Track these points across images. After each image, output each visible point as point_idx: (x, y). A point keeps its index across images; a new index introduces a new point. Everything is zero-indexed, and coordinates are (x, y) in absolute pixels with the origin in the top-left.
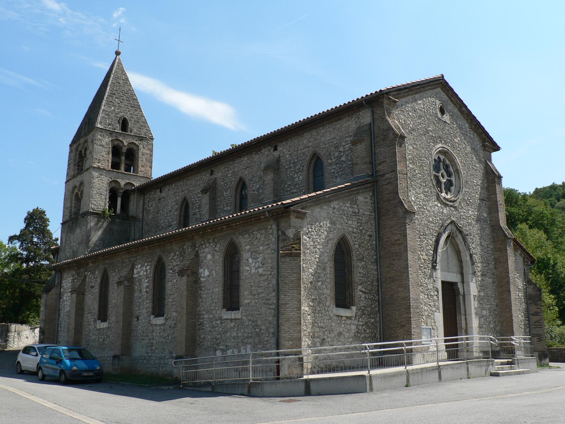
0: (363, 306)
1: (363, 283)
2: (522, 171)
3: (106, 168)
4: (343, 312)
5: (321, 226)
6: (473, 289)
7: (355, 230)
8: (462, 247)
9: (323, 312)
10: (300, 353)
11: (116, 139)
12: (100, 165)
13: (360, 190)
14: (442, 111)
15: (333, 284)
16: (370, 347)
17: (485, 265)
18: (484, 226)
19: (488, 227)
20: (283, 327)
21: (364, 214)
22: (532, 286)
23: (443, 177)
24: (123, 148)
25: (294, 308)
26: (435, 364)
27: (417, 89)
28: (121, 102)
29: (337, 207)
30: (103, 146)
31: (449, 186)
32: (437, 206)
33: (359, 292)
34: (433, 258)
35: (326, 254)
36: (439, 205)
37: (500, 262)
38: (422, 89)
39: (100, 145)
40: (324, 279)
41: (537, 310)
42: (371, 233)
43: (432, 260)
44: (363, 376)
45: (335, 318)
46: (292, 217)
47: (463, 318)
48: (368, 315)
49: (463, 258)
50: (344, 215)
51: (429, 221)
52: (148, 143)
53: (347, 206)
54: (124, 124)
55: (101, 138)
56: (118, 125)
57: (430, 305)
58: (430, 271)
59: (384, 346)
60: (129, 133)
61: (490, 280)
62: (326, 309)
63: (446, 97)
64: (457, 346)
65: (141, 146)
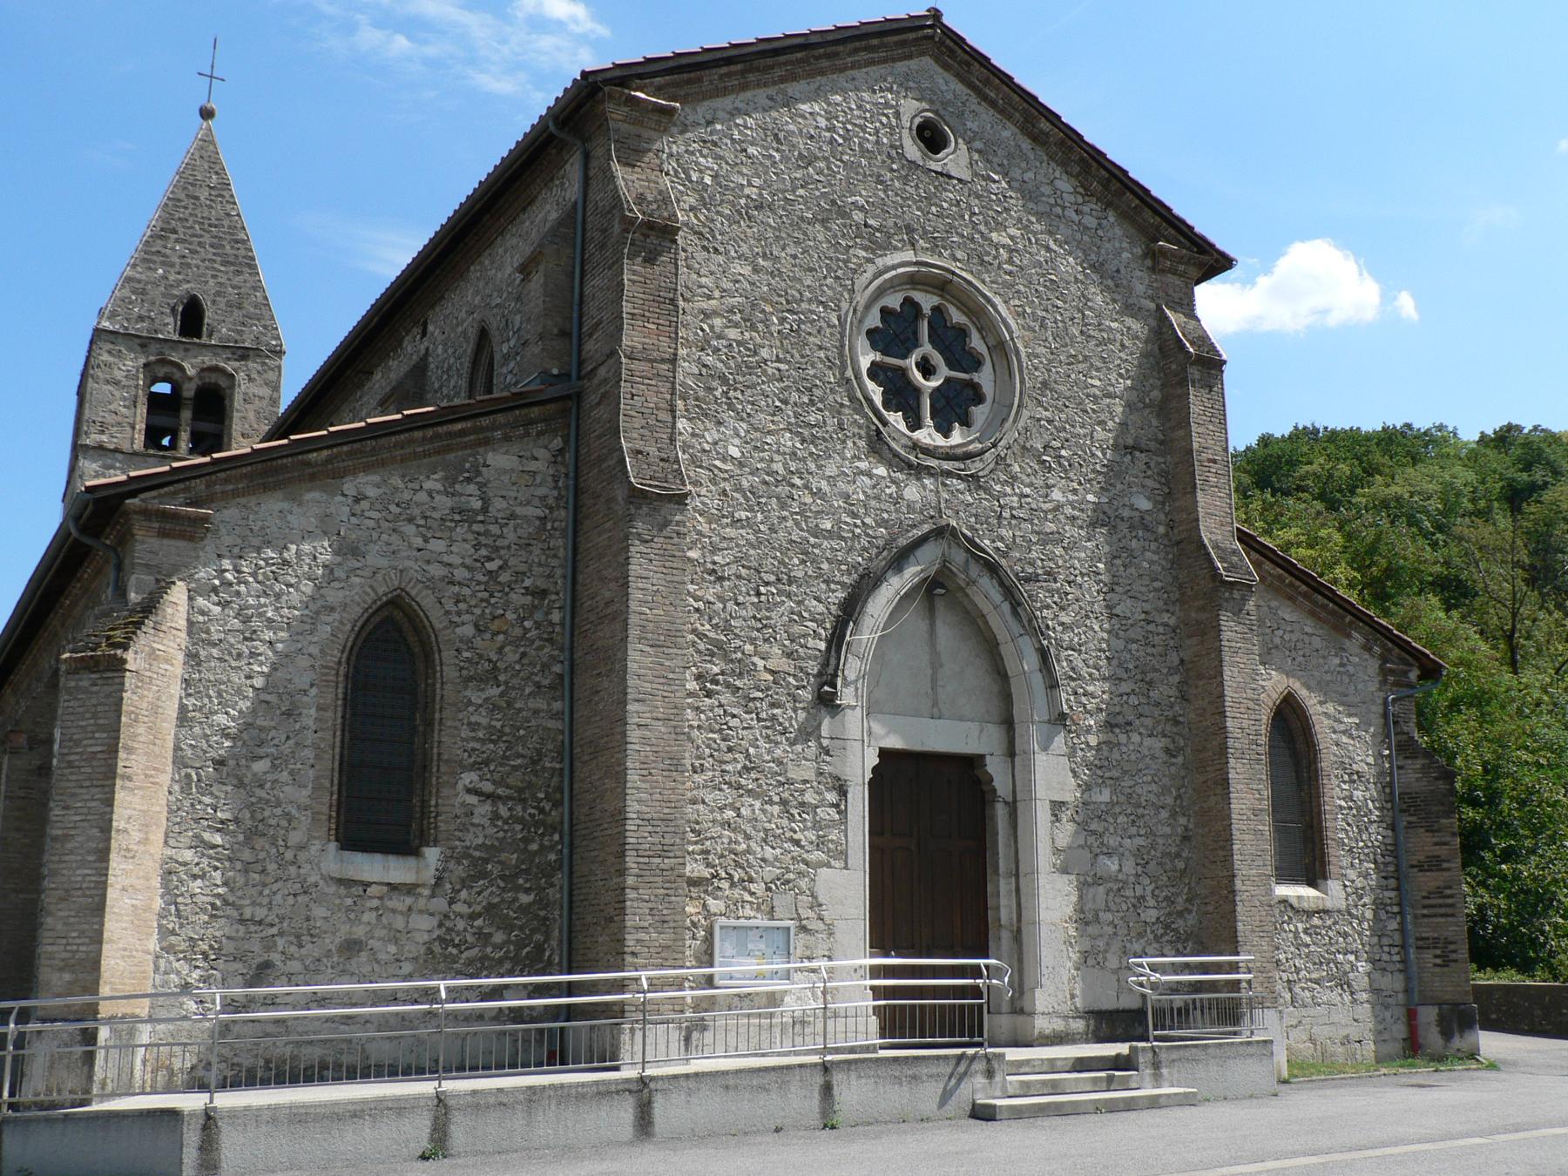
0: (477, 848)
1: (487, 763)
2: (1312, 330)
3: (126, 447)
4: (374, 868)
5: (286, 563)
6: (1052, 776)
7: (461, 574)
8: (1000, 621)
9: (272, 867)
10: (91, 1011)
11: (158, 361)
12: (104, 438)
13: (493, 428)
14: (931, 138)
15: (330, 762)
16: (518, 991)
17: (1125, 687)
18: (1134, 544)
19: (1153, 546)
20: (49, 920)
21: (513, 516)
22: (1419, 763)
23: (927, 369)
24: (186, 386)
25: (89, 853)
26: (815, 1059)
27: (792, 63)
28: (191, 251)
29: (372, 492)
30: (117, 383)
31: (954, 405)
32: (869, 475)
33: (463, 797)
34: (826, 664)
35: (303, 662)
36: (881, 471)
37: (1200, 676)
38: (825, 63)
39: (108, 382)
40: (286, 748)
41: (1437, 850)
42: (542, 584)
43: (820, 674)
44: (173, 1114)
45: (332, 889)
46: (139, 533)
47: (1005, 886)
48: (502, 877)
49: (1011, 666)
50: (411, 520)
51: (816, 532)
52: (264, 364)
53: (430, 490)
54: (192, 317)
55: (111, 359)
56: (170, 320)
57: (797, 843)
58: (802, 715)
59: (570, 988)
60: (204, 340)
61: (1148, 742)
62: (289, 855)
63: (960, 88)
64: (976, 992)
65: (241, 377)
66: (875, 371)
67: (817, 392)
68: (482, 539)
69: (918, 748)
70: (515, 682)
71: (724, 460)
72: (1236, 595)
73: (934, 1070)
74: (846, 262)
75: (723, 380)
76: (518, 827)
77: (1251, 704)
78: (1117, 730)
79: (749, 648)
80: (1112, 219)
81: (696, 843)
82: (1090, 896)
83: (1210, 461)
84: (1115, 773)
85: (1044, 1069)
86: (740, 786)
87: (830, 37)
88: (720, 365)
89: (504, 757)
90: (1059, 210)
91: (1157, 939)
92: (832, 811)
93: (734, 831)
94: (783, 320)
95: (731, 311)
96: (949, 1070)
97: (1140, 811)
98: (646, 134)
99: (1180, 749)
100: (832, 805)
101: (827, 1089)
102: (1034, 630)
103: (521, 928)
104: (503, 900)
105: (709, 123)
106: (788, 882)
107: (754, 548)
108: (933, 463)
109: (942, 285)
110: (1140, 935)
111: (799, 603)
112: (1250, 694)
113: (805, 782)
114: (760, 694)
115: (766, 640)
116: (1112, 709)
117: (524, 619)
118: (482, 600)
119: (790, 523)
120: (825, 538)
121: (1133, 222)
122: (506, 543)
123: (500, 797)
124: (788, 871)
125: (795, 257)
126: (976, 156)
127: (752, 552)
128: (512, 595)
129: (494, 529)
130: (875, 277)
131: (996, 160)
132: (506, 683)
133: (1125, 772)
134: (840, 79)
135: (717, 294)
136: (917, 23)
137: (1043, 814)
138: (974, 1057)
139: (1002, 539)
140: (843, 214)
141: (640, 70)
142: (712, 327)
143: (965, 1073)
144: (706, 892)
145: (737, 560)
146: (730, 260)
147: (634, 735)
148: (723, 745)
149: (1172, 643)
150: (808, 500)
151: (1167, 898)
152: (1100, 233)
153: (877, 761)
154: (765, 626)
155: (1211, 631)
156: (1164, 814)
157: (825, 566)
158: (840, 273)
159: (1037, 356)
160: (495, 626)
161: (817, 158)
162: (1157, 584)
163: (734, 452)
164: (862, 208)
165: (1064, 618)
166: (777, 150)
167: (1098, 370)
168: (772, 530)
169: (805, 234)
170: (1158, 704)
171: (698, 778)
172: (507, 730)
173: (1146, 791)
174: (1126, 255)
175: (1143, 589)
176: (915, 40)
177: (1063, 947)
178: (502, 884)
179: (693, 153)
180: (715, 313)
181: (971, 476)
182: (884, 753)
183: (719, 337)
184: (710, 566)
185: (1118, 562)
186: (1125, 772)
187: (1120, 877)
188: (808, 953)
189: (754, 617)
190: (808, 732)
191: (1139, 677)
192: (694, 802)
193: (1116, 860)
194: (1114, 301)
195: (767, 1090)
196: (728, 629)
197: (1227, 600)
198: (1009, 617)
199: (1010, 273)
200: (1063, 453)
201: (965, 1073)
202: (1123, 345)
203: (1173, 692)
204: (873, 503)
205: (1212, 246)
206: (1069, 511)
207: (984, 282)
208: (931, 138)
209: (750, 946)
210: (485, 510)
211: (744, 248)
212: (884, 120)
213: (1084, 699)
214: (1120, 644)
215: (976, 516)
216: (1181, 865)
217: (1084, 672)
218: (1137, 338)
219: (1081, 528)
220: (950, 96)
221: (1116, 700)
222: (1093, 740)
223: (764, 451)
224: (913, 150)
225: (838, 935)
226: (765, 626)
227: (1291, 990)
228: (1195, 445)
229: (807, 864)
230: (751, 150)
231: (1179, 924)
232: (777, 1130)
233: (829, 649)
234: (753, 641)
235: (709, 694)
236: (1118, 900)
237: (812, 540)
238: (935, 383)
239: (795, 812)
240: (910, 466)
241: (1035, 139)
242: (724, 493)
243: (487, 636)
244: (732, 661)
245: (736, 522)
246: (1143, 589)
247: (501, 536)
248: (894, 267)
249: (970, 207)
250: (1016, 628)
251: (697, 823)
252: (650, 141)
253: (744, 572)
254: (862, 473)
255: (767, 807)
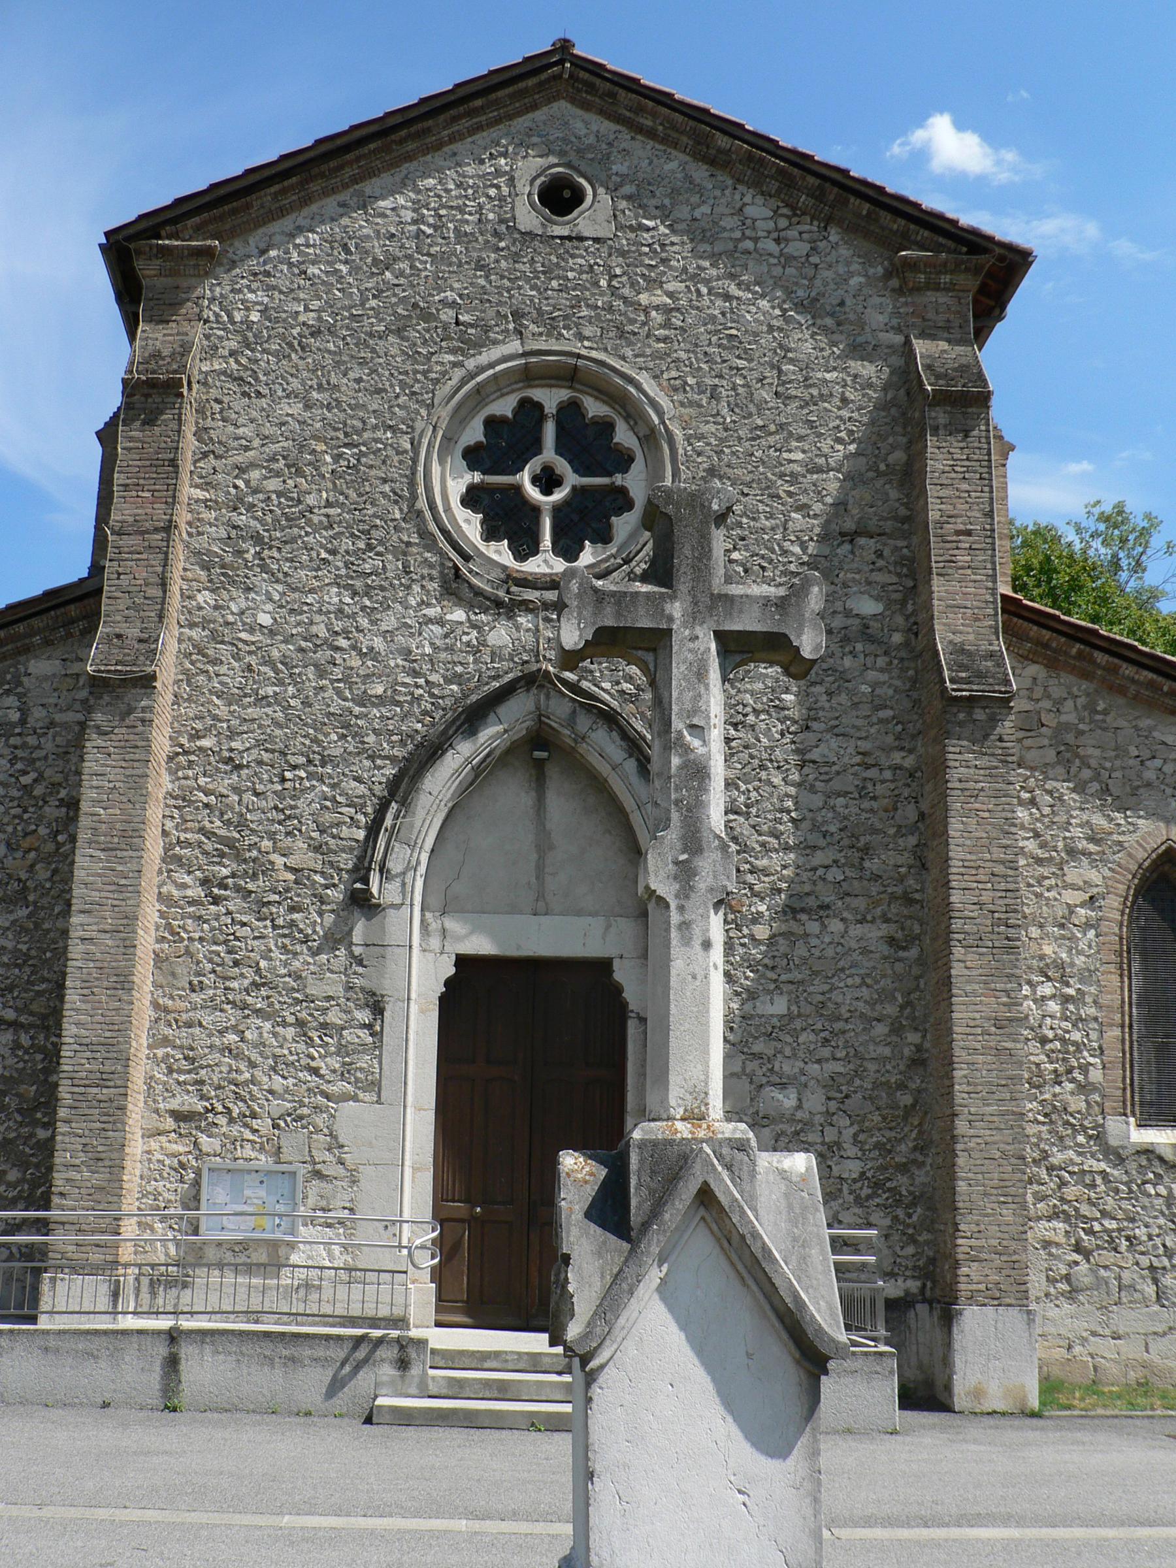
17: (819, 858)
18: (848, 662)
19: (881, 662)
21: (52, 724)
23: (548, 481)
34: (361, 859)
36: (459, 615)
48: (19, 1111)
57: (315, 1071)
61: (856, 931)
63: (607, 127)
66: (471, 499)
67: (375, 534)
68: (20, 753)
69: (512, 952)
70: (44, 901)
71: (251, 631)
72: (979, 714)
73: (320, 1352)
74: (425, 373)
75: (257, 539)
76: (39, 1057)
77: (999, 869)
78: (804, 917)
79: (266, 844)
81: (189, 1072)
83: (959, 533)
84: (796, 975)
85: (520, 1366)
86: (245, 1006)
88: (253, 523)
89: (28, 982)
91: (859, 1201)
92: (364, 1034)
93: (236, 1057)
94: (337, 458)
95: (273, 459)
96: (342, 1354)
98: (185, 284)
99: (912, 939)
100: (364, 1026)
101: (172, 1363)
103: (37, 1166)
104: (19, 1136)
105: (263, 252)
106: (301, 1118)
107: (280, 727)
108: (531, 595)
109: (569, 374)
111: (333, 786)
112: (998, 854)
113: (329, 998)
114: (277, 897)
115: (288, 834)
116: (798, 888)
117: (58, 832)
118: (15, 817)
119: (330, 693)
120: (374, 705)
122: (42, 753)
123: (22, 1026)
124: (302, 1104)
125: (359, 381)
126: (623, 204)
127: (278, 732)
128: (46, 809)
129: (32, 740)
130: (463, 382)
131: (654, 202)
132: (35, 903)
133: (815, 973)
134: (437, 159)
135: (257, 443)
136: (538, 64)
138: (380, 1341)
140: (427, 316)
141: (169, 215)
142: (247, 482)
143: (366, 1360)
144: (198, 1128)
145: (258, 744)
146: (276, 400)
147: (76, 950)
148: (229, 959)
150: (356, 662)
151: (878, 1146)
152: (814, 259)
153: (453, 971)
154: (289, 817)
155: (937, 769)
156: (880, 1029)
157: (371, 739)
159: (701, 437)
160: (25, 844)
161: (396, 259)
162: (887, 713)
163: (265, 619)
166: (346, 262)
167: (800, 438)
168: (306, 703)
169: (373, 351)
170: (876, 877)
171: (197, 998)
172: (33, 953)
174: (855, 281)
175: (859, 722)
178: (19, 1119)
179: (240, 291)
180: (253, 465)
183: (255, 491)
184: (226, 754)
186: (815, 973)
187: (799, 1115)
188: (323, 1203)
189: (276, 808)
190: (336, 939)
191: (846, 842)
194: (834, 344)
195: (95, 1357)
196: (242, 825)
197: (961, 724)
199: (665, 340)
201: (366, 1360)
202: (844, 400)
203: (905, 858)
205: (990, 239)
207: (624, 358)
208: (559, 197)
209: (247, 1193)
210: (23, 721)
211: (295, 384)
212: (492, 192)
213: (750, 878)
214: (817, 800)
216: (906, 1099)
217: (753, 841)
218: (870, 386)
220: (592, 140)
221: (805, 876)
222: (762, 932)
223: (302, 612)
224: (528, 217)
225: (362, 1184)
226: (289, 817)
227: (1156, 1281)
228: (933, 515)
229: (327, 1097)
230: (313, 270)
231: (901, 1182)
232: (105, 1405)
233: (367, 838)
234: (272, 836)
235: (216, 901)
237: (357, 710)
238: (558, 496)
239: (314, 1035)
240: (498, 604)
241: (712, 162)
242: (249, 668)
243: (19, 854)
244: (245, 861)
245: (261, 700)
246: (859, 722)
247: (39, 747)
248: (491, 365)
251: (192, 1049)
252: (191, 289)
253: (266, 756)
254: (430, 621)
255: (279, 1029)
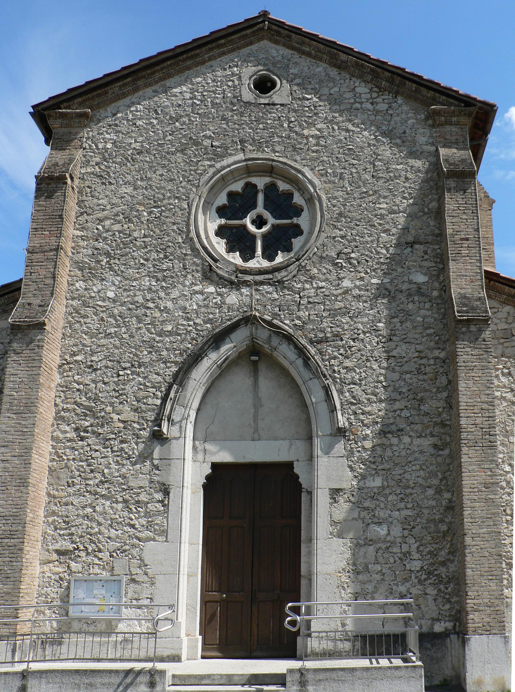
18: (410, 306)
23: (259, 222)
36: (211, 289)
57: (133, 526)
61: (417, 442)
63: (287, 52)
69: (241, 460)
71: (104, 300)
73: (106, 680)
74: (195, 171)
77: (485, 406)
78: (390, 436)
79: (109, 409)
80: (400, 101)
81: (66, 529)
82: (361, 553)
83: (462, 239)
85: (222, 682)
86: (96, 493)
87: (190, 47)
88: (106, 247)
90: (358, 105)
93: (91, 520)
94: (150, 213)
95: (117, 215)
96: (118, 681)
97: (408, 491)
98: (74, 131)
100: (159, 501)
102: (317, 374)
106: (125, 551)
109: (269, 169)
110: (406, 580)
111: (145, 378)
112: (484, 398)
113: (141, 488)
114: (114, 436)
115: (121, 403)
116: (387, 421)
119: (144, 330)
120: (167, 336)
121: (416, 99)
124: (125, 544)
125: (161, 175)
127: (116, 351)
130: (215, 174)
133: (396, 464)
134: (202, 68)
135: (109, 207)
136: (252, 23)
137: (322, 499)
139: (299, 318)
140: (196, 143)
142: (103, 227)
143: (131, 684)
144: (70, 559)
145: (106, 357)
148: (88, 469)
149: (441, 370)
150: (157, 314)
151: (430, 553)
156: (430, 492)
157: (165, 353)
158: (191, 178)
159: (335, 198)
161: (181, 116)
163: (111, 294)
164: (210, 137)
165: (348, 363)
167: (385, 197)
169: (169, 160)
170: (427, 414)
171: (70, 490)
173: (414, 475)
174: (411, 122)
175: (417, 336)
176: (254, 32)
177: (337, 590)
179: (102, 134)
180: (106, 218)
181: (278, 281)
182: (215, 466)
183: (107, 231)
184: (89, 363)
185: (395, 320)
186: (396, 464)
188: (136, 596)
189: (114, 390)
190: (145, 456)
191: (411, 397)
192: (66, 504)
193: (385, 527)
196: (96, 399)
197: (463, 333)
198: (302, 369)
199: (316, 151)
200: (353, 255)
201: (131, 684)
202: (407, 178)
204: (203, 310)
205: (475, 99)
206: (356, 292)
207: (296, 161)
208: (264, 85)
211: (129, 178)
213: (362, 417)
215: (279, 306)
216: (444, 528)
217: (363, 398)
218: (419, 171)
219: (366, 302)
220: (280, 58)
221: (391, 415)
222: (368, 444)
224: (248, 94)
225: (157, 585)
228: (449, 231)
229: (139, 539)
230: (139, 123)
234: (112, 404)
235: (82, 439)
236: (386, 555)
237: (158, 338)
239: (133, 507)
240: (232, 283)
241: (339, 67)
242: (102, 319)
244: (98, 418)
245: (108, 335)
248: (229, 166)
249: (288, 119)
250: (307, 375)
251: (67, 517)
252: (77, 133)
253: (110, 364)
254: (196, 292)
